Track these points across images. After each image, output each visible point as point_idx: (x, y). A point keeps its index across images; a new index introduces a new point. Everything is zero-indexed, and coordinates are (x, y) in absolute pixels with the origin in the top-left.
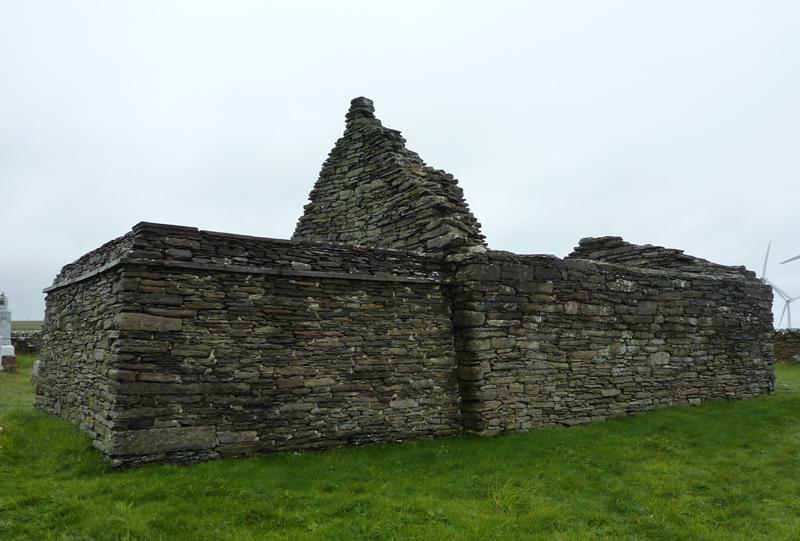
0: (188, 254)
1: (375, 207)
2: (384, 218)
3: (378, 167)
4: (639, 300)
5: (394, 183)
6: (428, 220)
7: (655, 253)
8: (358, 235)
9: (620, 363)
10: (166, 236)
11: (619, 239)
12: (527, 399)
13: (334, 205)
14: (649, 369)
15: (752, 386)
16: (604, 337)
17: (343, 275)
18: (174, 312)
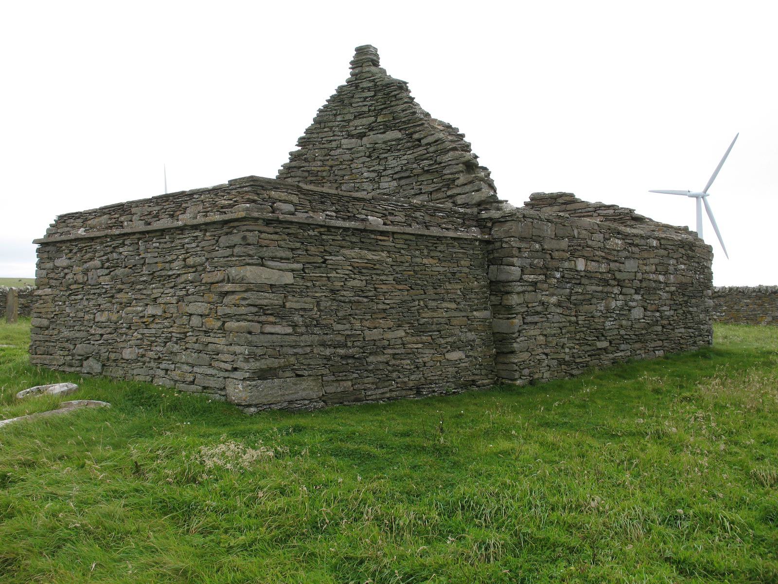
0: (291, 208)
1: (390, 158)
2: (402, 171)
3: (394, 119)
4: (626, 258)
5: (416, 136)
6: (457, 176)
7: (611, 212)
8: (368, 186)
9: (611, 317)
10: (271, 190)
11: (572, 195)
12: (547, 351)
13: (332, 153)
14: (630, 323)
15: (698, 339)
16: (602, 292)
17: (408, 230)
18: (284, 266)
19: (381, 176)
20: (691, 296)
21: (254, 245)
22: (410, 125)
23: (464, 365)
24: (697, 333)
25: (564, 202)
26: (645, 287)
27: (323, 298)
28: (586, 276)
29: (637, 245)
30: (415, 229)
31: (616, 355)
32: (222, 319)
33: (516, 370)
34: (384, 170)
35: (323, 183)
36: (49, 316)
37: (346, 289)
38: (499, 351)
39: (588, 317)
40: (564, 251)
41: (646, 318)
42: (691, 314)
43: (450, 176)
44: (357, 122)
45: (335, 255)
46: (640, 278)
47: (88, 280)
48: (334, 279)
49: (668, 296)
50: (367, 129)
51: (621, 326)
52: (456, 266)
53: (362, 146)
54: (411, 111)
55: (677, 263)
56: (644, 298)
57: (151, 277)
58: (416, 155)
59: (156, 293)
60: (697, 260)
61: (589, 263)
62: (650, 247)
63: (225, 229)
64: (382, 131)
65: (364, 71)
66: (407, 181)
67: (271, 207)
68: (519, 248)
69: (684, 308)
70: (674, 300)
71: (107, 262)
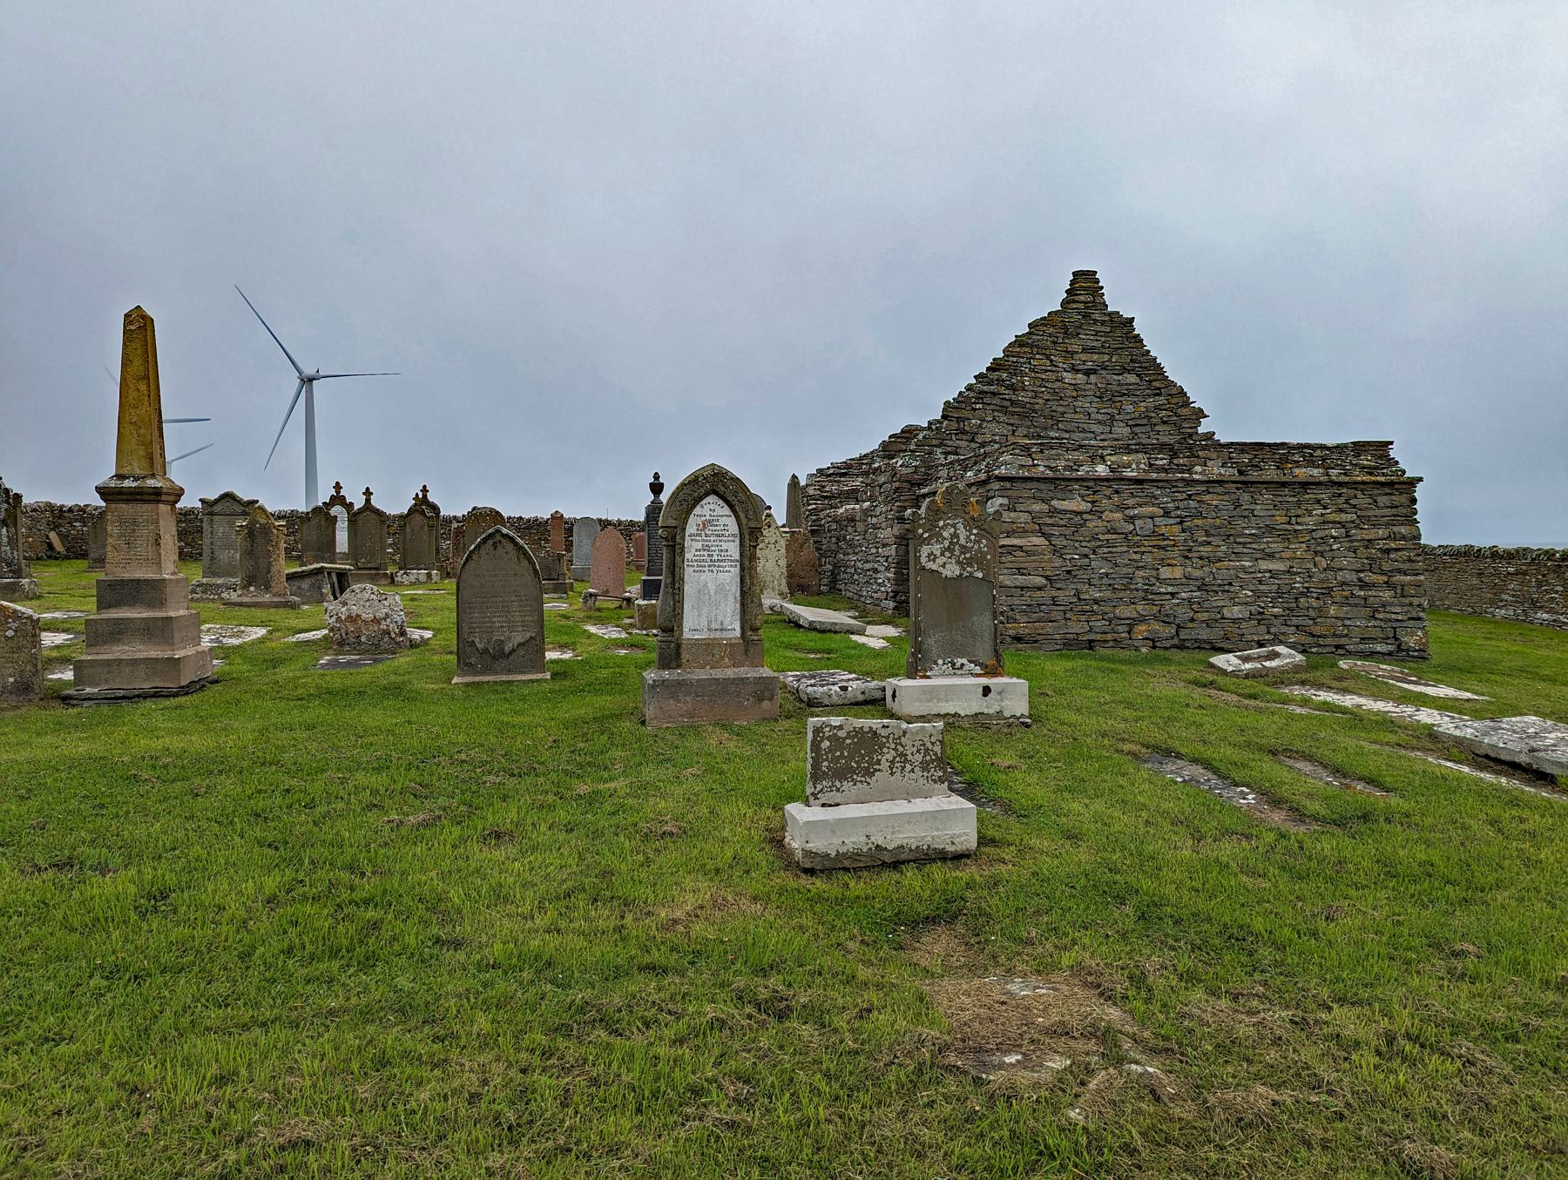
43: (1189, 430)
44: (1083, 357)
66: (1143, 429)
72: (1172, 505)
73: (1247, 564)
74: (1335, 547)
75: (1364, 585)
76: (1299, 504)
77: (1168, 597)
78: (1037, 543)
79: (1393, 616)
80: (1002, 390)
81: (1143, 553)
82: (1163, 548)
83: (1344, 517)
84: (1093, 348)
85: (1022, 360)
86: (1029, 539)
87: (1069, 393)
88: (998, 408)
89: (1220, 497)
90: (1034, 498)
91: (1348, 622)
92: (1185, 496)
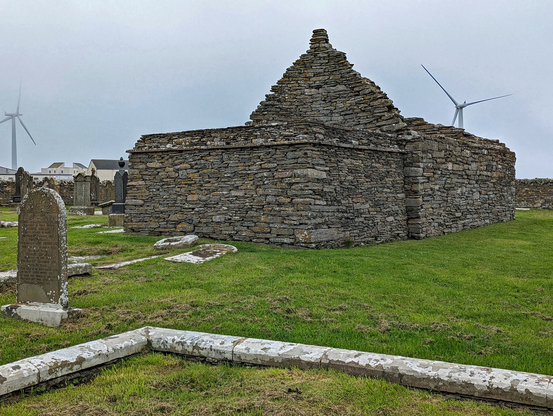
5: (356, 89)
9: (463, 198)
19: (332, 113)
20: (504, 185)
21: (310, 157)
22: (352, 82)
23: (394, 224)
24: (507, 209)
25: (416, 124)
26: (481, 180)
27: (337, 186)
28: (452, 173)
29: (477, 154)
30: (372, 146)
31: (465, 221)
32: (291, 198)
33: (420, 228)
34: (335, 109)
35: (291, 116)
36: (144, 198)
37: (346, 181)
38: (410, 217)
39: (453, 198)
40: (442, 158)
41: (481, 199)
42: (504, 197)
43: (379, 114)
44: (314, 79)
45: (341, 163)
46: (479, 174)
47: (179, 176)
48: (341, 176)
49: (492, 185)
50: (323, 83)
51: (468, 203)
52: (389, 168)
53: (319, 94)
54: (353, 73)
55: (497, 164)
56: (480, 186)
57: (233, 174)
58: (357, 100)
59: (239, 183)
60: (507, 162)
61: (454, 165)
62: (483, 155)
63: (291, 149)
64: (333, 85)
65: (321, 46)
66: (350, 116)
67: (314, 136)
68: (422, 157)
69: (500, 193)
70: (496, 188)
71: (195, 165)
72: (193, 162)
73: (225, 193)
74: (266, 182)
75: (279, 205)
76: (250, 159)
77: (191, 210)
78: (141, 184)
79: (292, 222)
80: (276, 103)
81: (181, 188)
82: (190, 185)
83: (271, 165)
84: (319, 73)
85: (284, 85)
86: (138, 182)
87: (308, 100)
88: (274, 113)
89: (214, 157)
90: (141, 162)
91: (271, 225)
92: (199, 157)
